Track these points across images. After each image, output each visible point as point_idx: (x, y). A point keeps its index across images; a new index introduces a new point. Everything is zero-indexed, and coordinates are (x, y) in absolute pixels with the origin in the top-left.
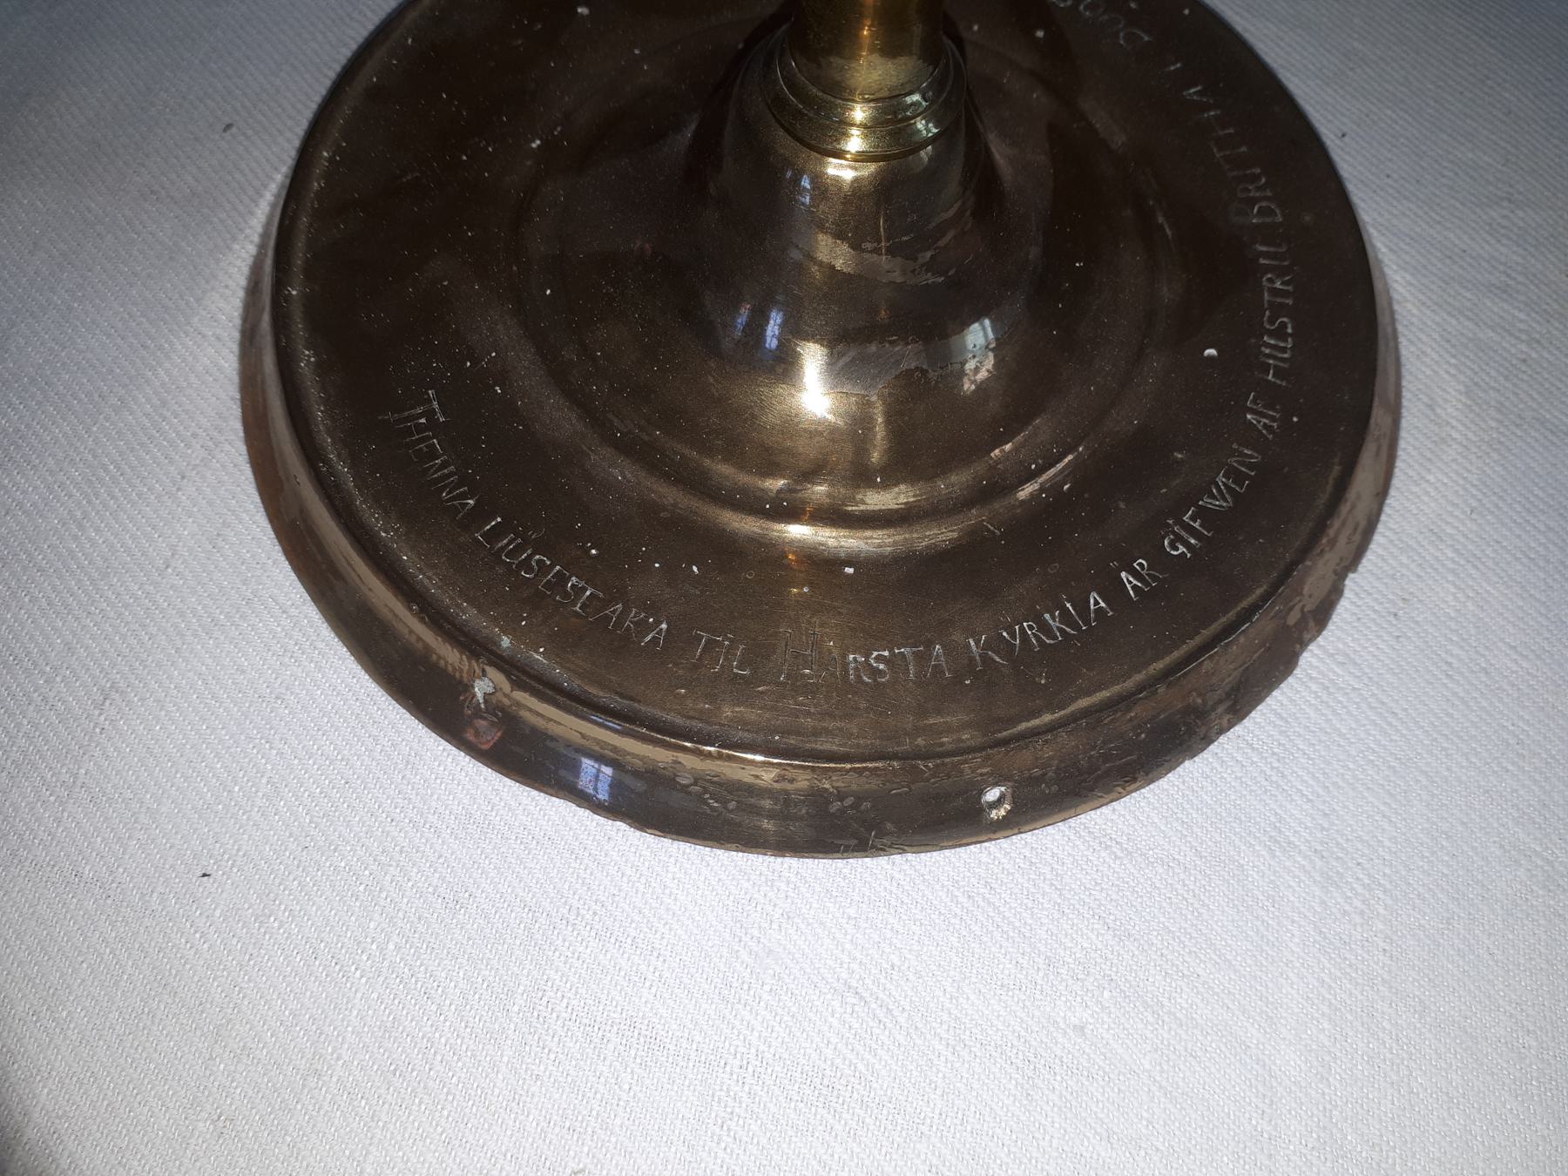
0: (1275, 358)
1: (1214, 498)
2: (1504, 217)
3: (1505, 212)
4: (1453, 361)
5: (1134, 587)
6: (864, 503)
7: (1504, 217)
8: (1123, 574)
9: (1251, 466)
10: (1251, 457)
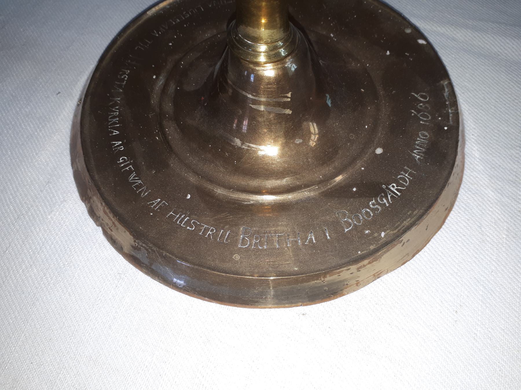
0: (179, 218)
1: (135, 177)
2: (517, 153)
3: (517, 152)
4: (491, 209)
5: (115, 144)
6: (335, 181)
7: (517, 153)
8: (121, 142)
9: (140, 192)
10: (144, 194)
